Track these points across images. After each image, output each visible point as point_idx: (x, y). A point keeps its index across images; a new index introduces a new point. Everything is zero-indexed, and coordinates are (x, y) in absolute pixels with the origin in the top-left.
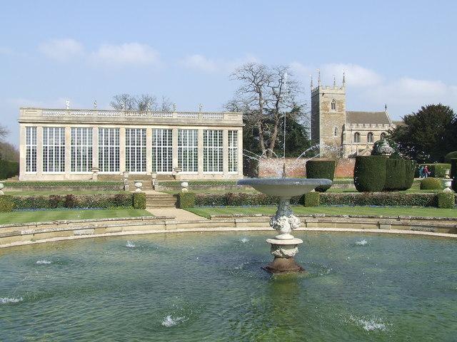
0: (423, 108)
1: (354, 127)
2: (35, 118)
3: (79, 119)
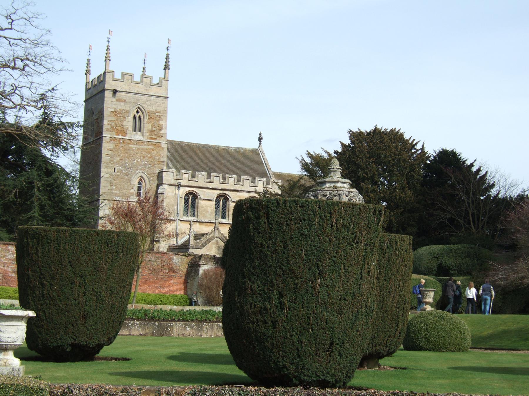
1: (186, 177)
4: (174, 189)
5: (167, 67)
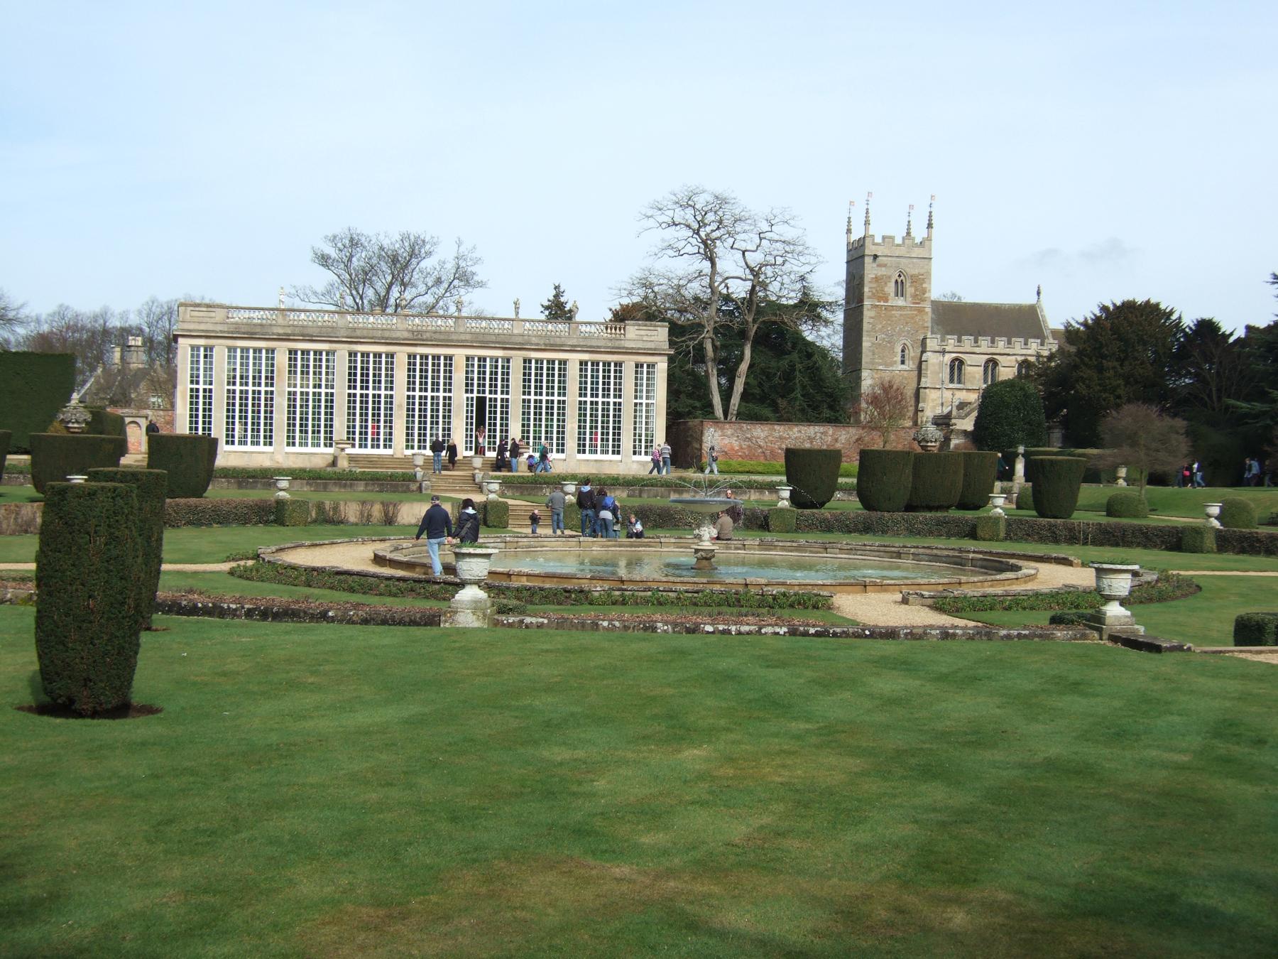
1: (951, 342)
2: (211, 327)
3: (306, 331)
4: (940, 357)
5: (930, 226)
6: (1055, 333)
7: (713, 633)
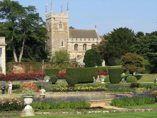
0: (115, 30)
1: (74, 40)
6: (100, 37)
7: (91, 113)
